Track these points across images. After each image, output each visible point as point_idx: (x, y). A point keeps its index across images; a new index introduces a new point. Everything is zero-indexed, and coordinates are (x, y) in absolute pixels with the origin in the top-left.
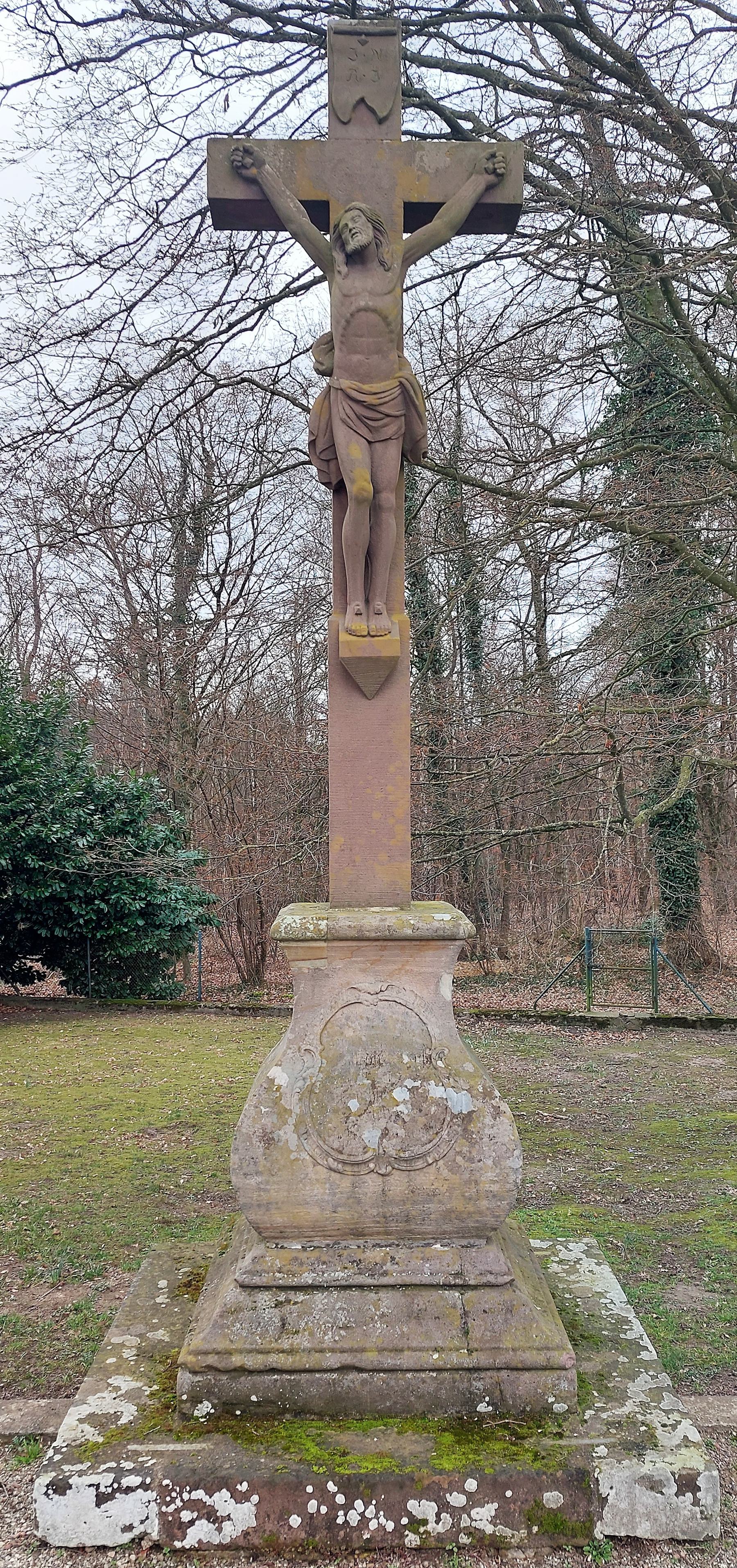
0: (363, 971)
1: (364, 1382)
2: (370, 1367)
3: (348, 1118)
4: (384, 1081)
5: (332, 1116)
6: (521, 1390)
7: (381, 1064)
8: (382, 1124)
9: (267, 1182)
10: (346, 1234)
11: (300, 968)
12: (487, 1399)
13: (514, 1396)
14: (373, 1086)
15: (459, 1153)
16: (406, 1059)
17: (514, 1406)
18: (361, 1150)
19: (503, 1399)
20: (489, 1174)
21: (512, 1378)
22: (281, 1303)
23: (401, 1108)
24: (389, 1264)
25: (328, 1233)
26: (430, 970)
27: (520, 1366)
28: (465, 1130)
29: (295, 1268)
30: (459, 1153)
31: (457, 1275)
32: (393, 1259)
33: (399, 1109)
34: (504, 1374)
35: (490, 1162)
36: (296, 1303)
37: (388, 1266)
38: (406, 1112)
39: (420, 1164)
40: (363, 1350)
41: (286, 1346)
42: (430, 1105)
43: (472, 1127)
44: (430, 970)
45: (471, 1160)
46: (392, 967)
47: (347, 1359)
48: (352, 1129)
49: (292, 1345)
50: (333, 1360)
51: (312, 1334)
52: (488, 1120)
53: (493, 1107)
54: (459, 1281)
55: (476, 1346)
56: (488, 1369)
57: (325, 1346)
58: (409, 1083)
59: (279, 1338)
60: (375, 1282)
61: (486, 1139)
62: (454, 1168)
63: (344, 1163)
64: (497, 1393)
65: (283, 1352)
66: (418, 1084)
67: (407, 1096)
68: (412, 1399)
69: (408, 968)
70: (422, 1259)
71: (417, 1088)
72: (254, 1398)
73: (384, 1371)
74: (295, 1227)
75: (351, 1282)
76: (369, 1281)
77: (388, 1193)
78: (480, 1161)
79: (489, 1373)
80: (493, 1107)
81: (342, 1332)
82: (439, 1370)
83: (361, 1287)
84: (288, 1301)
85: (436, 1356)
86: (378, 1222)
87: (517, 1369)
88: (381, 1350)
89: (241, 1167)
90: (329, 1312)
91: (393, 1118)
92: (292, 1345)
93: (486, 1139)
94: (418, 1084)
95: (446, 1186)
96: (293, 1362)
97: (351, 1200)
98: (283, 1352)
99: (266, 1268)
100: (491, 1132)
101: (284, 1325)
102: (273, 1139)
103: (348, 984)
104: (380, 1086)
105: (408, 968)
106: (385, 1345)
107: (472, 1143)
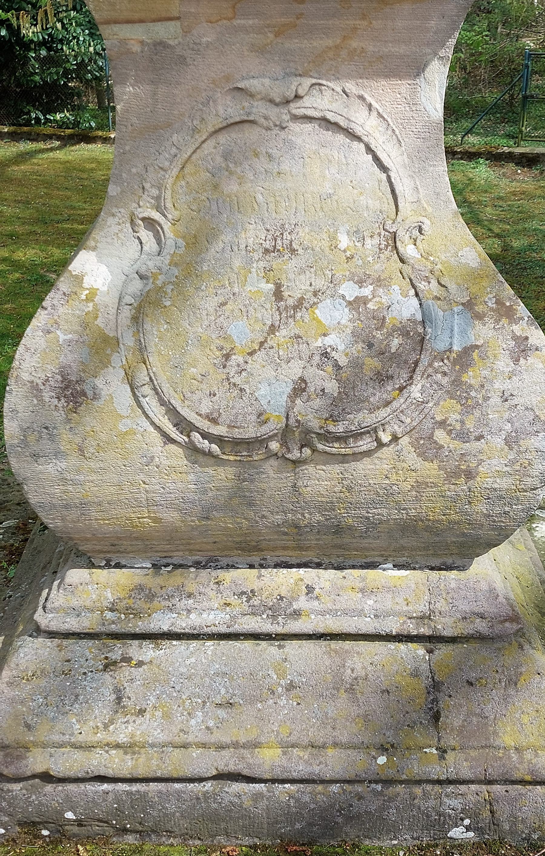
0: (260, 50)
1: (257, 797)
2: (267, 776)
3: (227, 357)
4: (297, 287)
5: (196, 352)
6: (526, 812)
7: (293, 251)
8: (295, 370)
9: (78, 471)
10: (230, 549)
11: (123, 42)
12: (467, 822)
13: (514, 820)
14: (278, 294)
15: (442, 424)
16: (344, 241)
17: (512, 832)
18: (254, 418)
19: (495, 823)
20: (494, 462)
21: (513, 793)
22: (115, 663)
23: (331, 340)
24: (303, 598)
25: (197, 547)
26: (402, 49)
27: (528, 778)
28: (457, 383)
29: (140, 604)
30: (442, 424)
31: (422, 618)
32: (310, 589)
33: (329, 341)
34: (498, 788)
35: (498, 441)
36: (140, 664)
37: (302, 603)
38: (341, 347)
39: (365, 444)
40: (256, 745)
41: (122, 738)
42: (390, 334)
43: (470, 377)
44: (402, 49)
45: (463, 436)
46: (321, 43)
47: (228, 761)
48: (237, 380)
49: (132, 736)
50: (206, 763)
51: (167, 716)
52: (503, 364)
53: (515, 338)
54: (424, 630)
55: (453, 743)
56: (472, 782)
57: (191, 738)
58: (350, 290)
59: (112, 722)
60: (280, 630)
61: (495, 400)
62: (427, 448)
63: (219, 440)
64: (487, 814)
65: (118, 746)
66: (367, 291)
67: (344, 315)
68: (340, 820)
69: (354, 44)
70: (362, 590)
71: (364, 301)
72: (69, 815)
73: (293, 781)
74: (137, 539)
75: (237, 628)
76: (268, 627)
77: (303, 490)
78: (479, 438)
79: (473, 787)
80: (515, 338)
81: (222, 713)
82: (388, 782)
83: (256, 636)
84: (127, 660)
85: (382, 760)
86: (285, 534)
87: (522, 782)
88: (287, 746)
89: (24, 443)
90: (197, 680)
91: (317, 358)
92: (132, 736)
93: (495, 400)
94: (367, 291)
95: (412, 481)
96: (135, 767)
97: (236, 501)
98: (118, 746)
99: (88, 603)
100: (507, 385)
101: (119, 699)
102: (84, 394)
103: (228, 78)
104: (292, 294)
105: (354, 44)
106: (293, 739)
107: (468, 407)
